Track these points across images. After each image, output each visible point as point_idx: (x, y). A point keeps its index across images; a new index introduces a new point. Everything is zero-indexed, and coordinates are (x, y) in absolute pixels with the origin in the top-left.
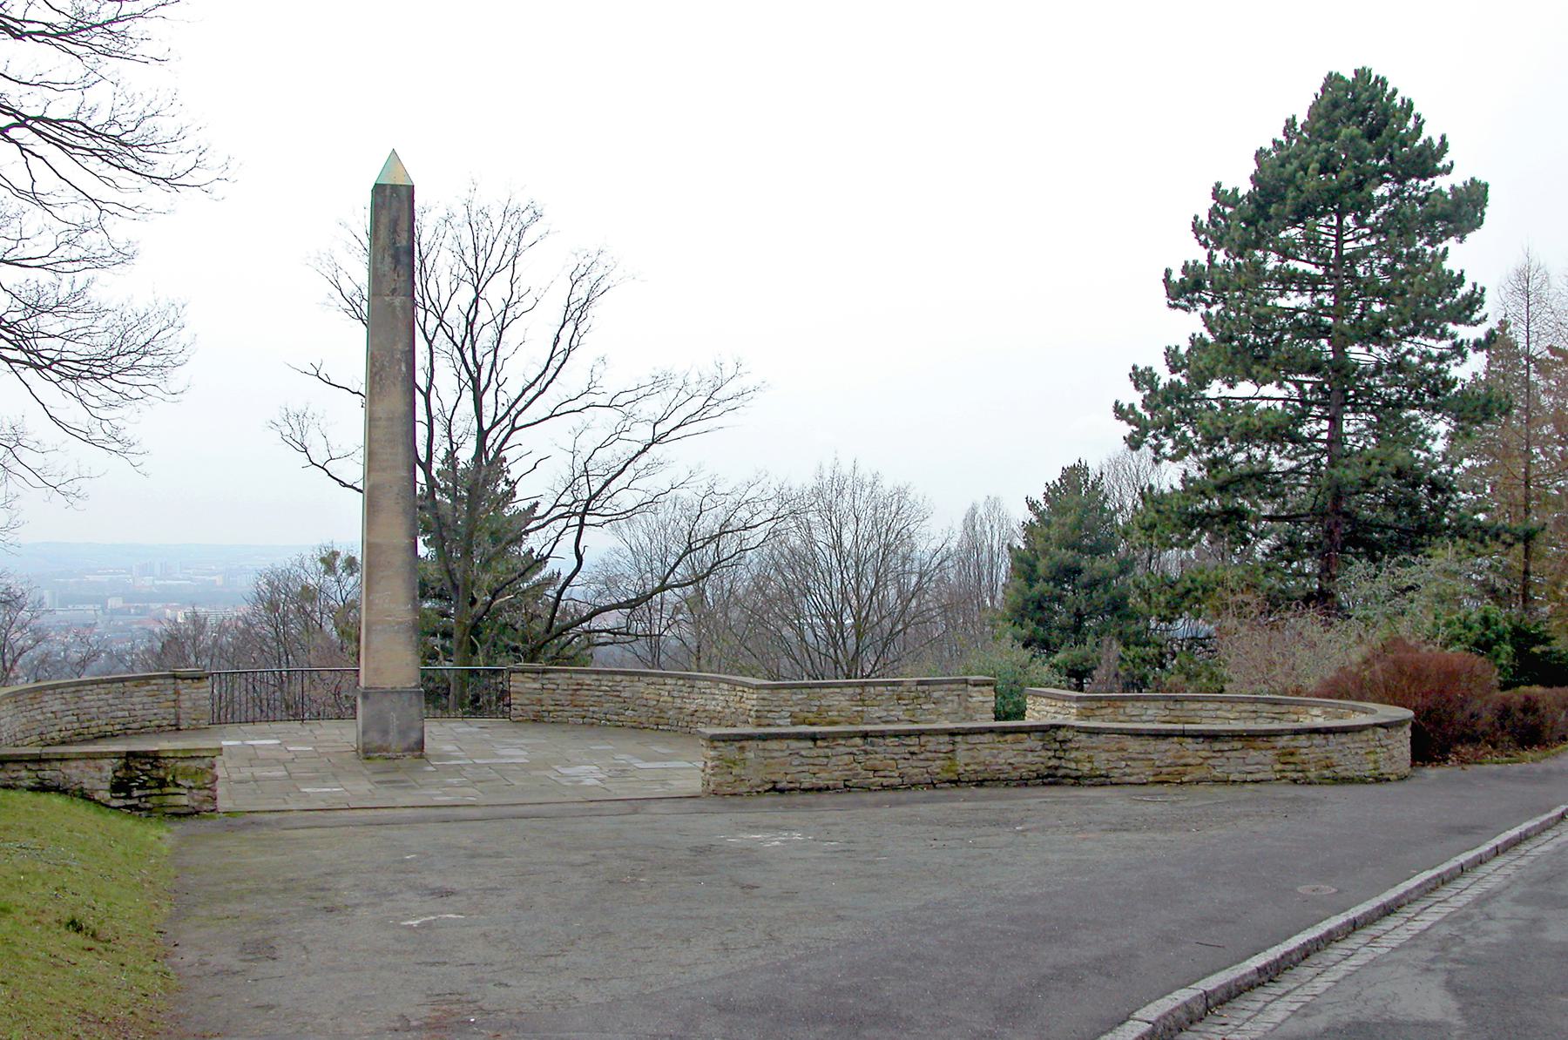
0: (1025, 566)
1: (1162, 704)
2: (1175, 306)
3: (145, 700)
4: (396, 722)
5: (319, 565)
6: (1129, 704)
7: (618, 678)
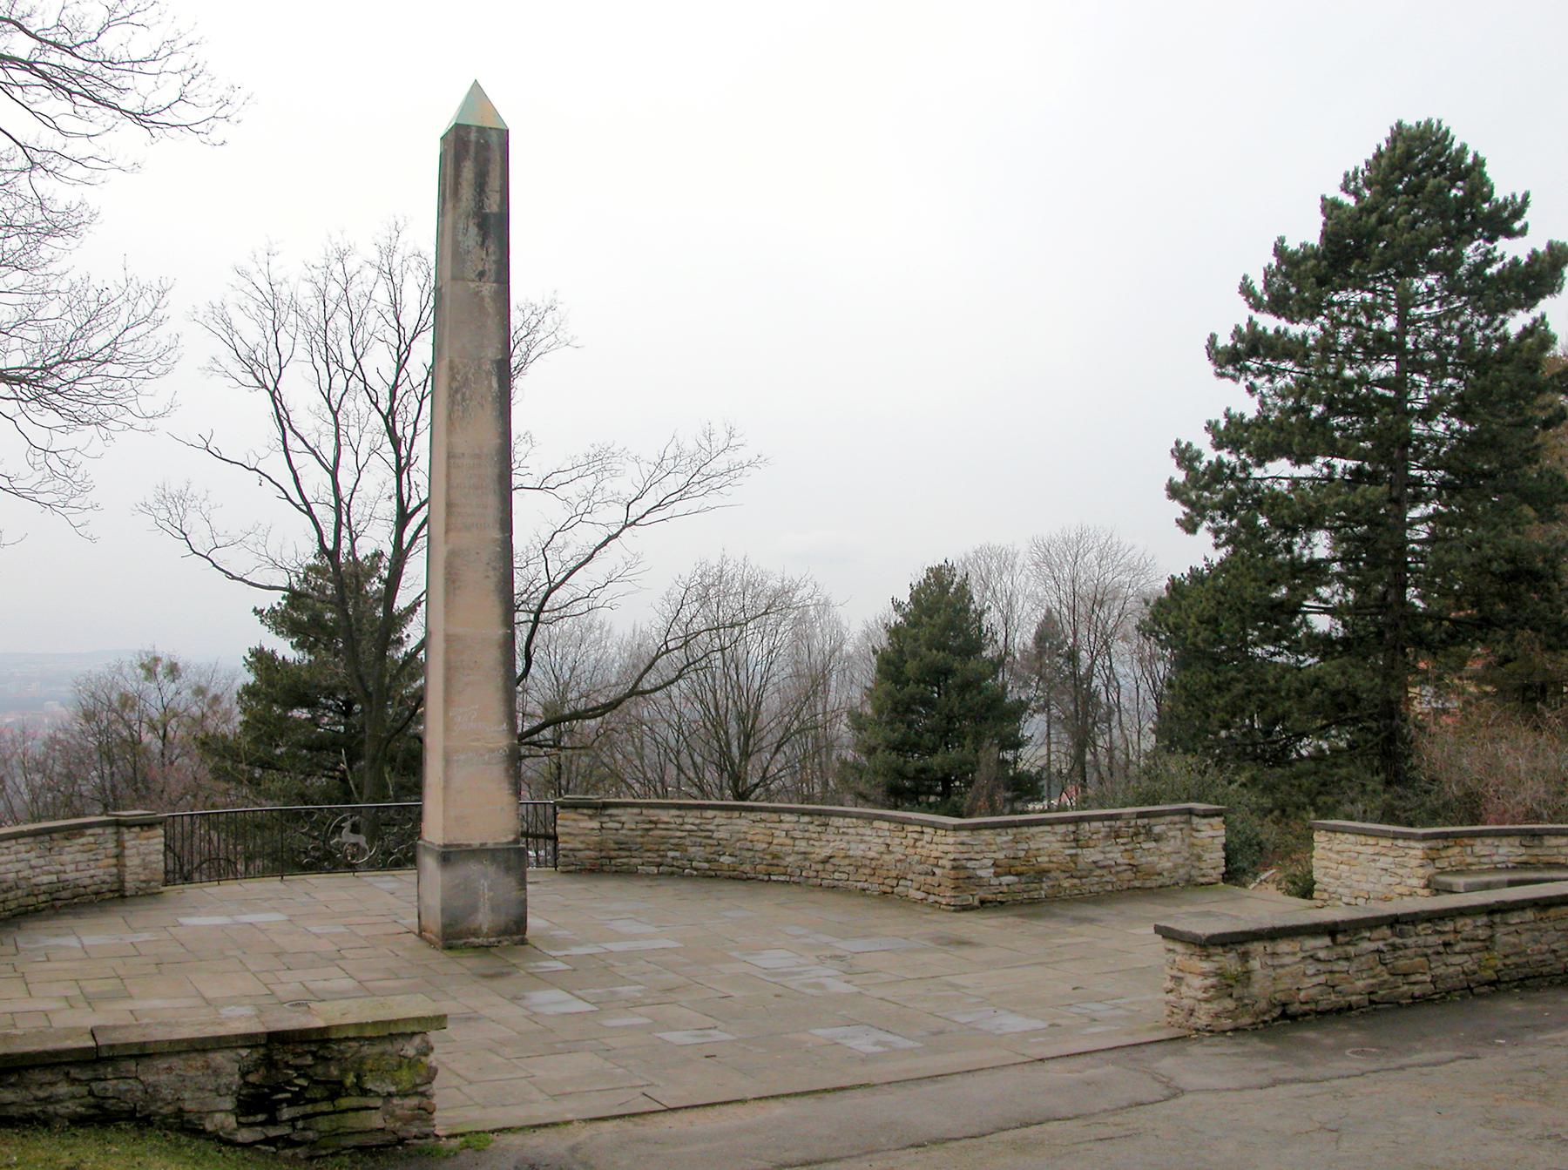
0: (891, 665)
1: (1516, 841)
2: (1222, 375)
3: (79, 857)
4: (488, 894)
5: (139, 670)
6: (1478, 842)
7: (710, 814)
